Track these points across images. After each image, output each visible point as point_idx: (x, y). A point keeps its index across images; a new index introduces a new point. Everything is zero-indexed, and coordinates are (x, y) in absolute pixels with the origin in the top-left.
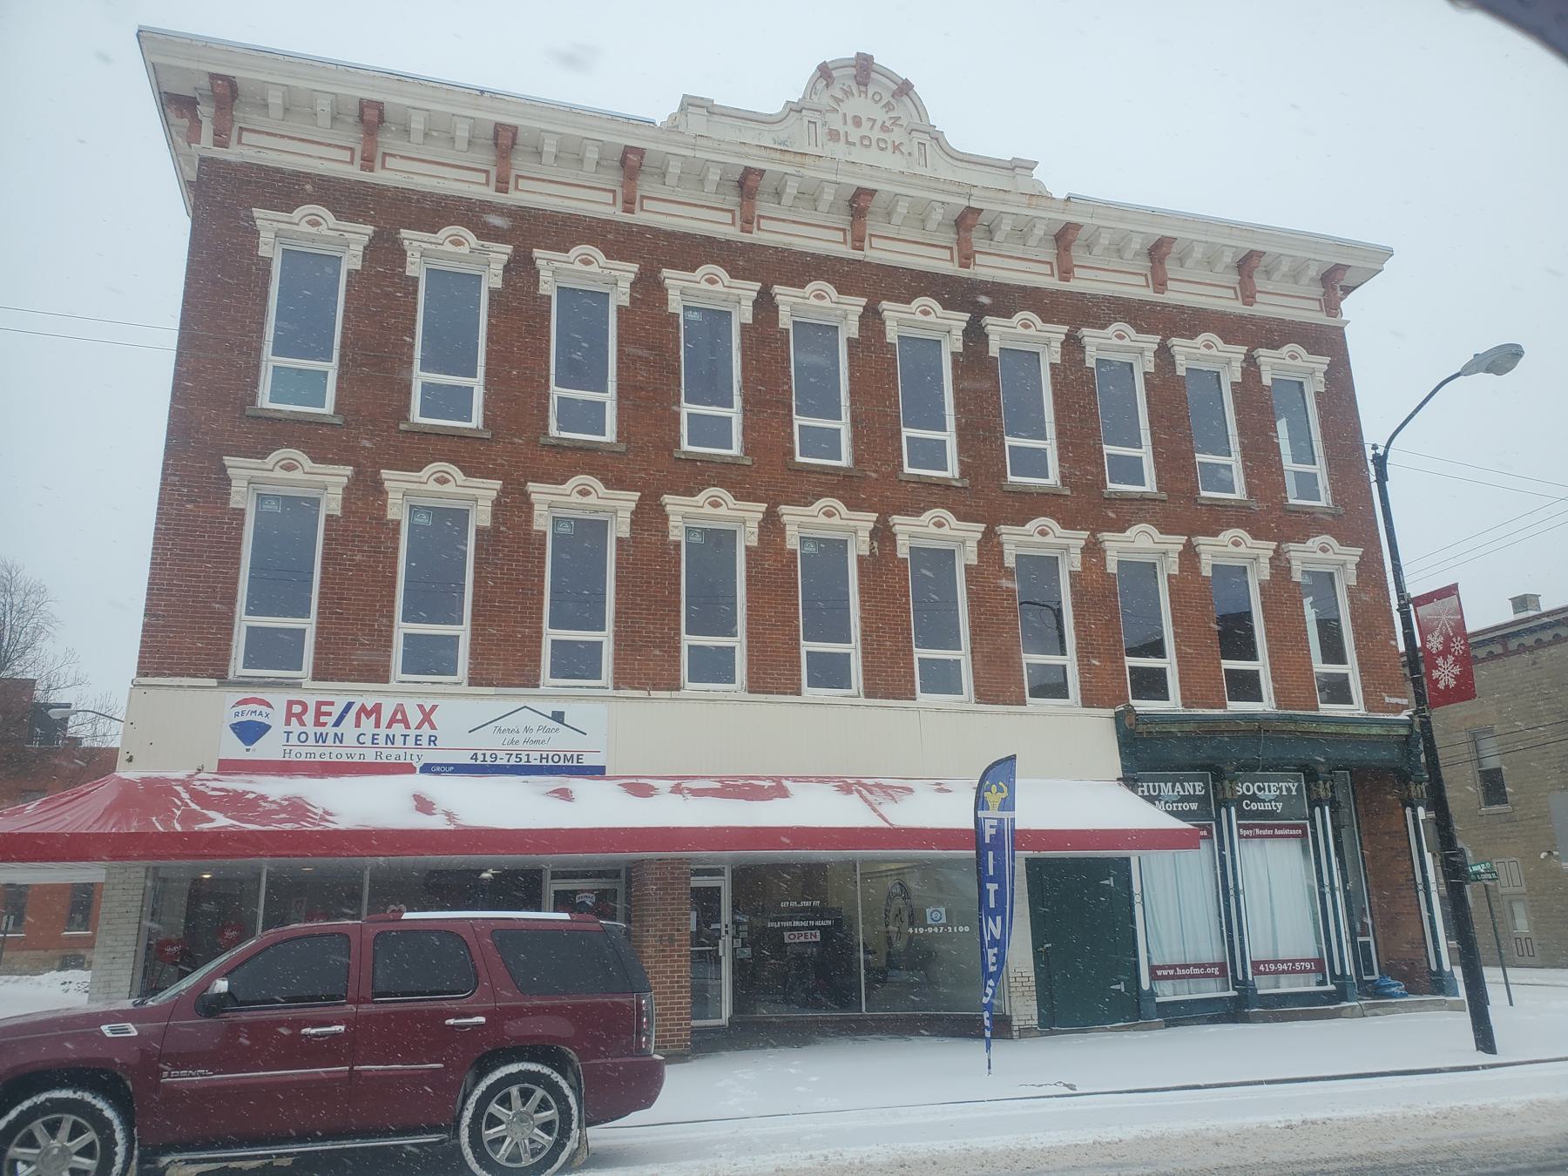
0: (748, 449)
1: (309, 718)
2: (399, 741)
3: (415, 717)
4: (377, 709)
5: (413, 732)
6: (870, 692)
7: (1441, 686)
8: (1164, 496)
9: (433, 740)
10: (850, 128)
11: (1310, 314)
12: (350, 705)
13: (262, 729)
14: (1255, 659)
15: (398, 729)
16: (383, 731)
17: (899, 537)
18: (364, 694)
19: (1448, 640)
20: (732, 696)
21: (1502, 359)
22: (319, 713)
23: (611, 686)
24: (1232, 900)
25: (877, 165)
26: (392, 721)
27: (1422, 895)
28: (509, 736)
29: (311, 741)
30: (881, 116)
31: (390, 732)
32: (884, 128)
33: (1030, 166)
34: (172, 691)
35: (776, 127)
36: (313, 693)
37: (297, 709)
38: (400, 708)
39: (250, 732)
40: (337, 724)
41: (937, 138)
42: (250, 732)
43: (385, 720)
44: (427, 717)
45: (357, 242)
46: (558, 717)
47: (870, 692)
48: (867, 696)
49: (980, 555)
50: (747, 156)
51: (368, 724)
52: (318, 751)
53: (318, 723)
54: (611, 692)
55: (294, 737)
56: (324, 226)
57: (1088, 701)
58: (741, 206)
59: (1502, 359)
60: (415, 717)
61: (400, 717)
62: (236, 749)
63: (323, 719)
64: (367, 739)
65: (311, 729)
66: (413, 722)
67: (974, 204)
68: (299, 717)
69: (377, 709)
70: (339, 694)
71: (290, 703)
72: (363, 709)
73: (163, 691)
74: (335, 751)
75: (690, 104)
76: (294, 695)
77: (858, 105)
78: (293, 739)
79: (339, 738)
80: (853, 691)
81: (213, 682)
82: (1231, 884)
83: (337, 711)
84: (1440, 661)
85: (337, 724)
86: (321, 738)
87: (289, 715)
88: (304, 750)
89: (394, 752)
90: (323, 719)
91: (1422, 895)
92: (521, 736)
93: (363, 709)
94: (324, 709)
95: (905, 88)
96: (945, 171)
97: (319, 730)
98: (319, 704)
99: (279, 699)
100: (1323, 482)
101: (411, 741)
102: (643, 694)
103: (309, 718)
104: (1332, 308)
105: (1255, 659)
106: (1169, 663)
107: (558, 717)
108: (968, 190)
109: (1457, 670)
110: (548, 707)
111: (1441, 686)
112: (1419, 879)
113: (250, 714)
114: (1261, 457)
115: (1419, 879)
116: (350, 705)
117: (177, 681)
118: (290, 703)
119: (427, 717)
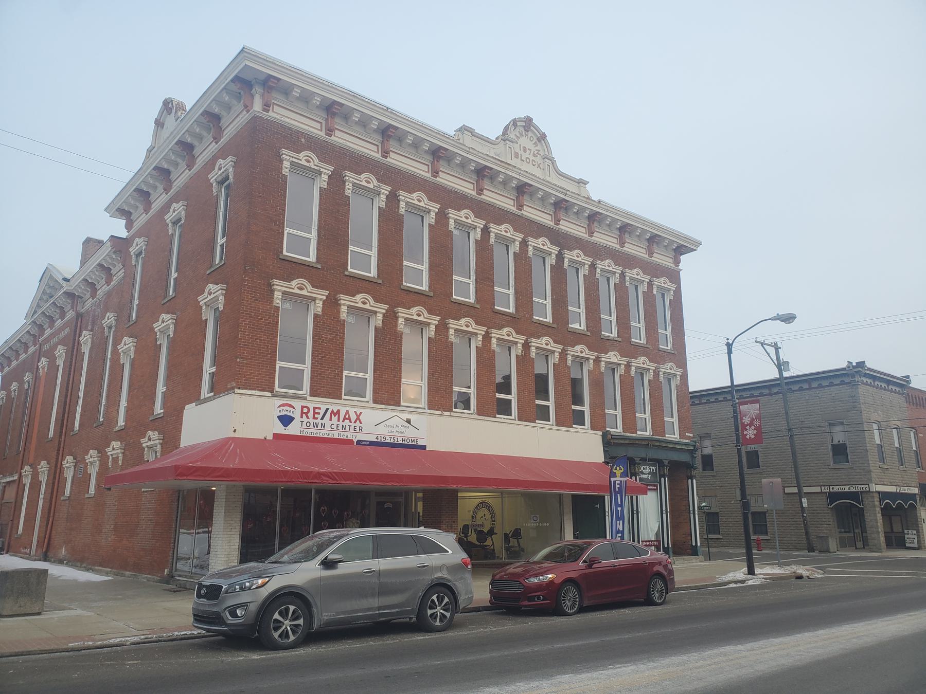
0: (478, 300)
1: (311, 415)
2: (347, 428)
3: (353, 417)
4: (338, 411)
5: (353, 425)
6: (558, 424)
7: (748, 437)
8: (620, 339)
9: (361, 429)
10: (522, 152)
11: (667, 262)
12: (327, 409)
13: (292, 419)
14: (510, 394)
15: (347, 421)
16: (341, 423)
17: (276, 293)
18: (332, 405)
19: (752, 420)
20: (367, 405)
21: (788, 319)
22: (315, 413)
23: (371, 402)
24: (635, 516)
25: (528, 169)
26: (345, 418)
27: (692, 515)
28: (391, 429)
29: (312, 426)
30: (533, 149)
31: (344, 424)
32: (534, 155)
33: (585, 183)
34: (252, 397)
35: (495, 147)
36: (313, 402)
37: (305, 410)
38: (347, 412)
39: (286, 420)
40: (322, 419)
41: (553, 161)
42: (286, 420)
43: (341, 419)
44: (358, 418)
45: (325, 174)
46: (409, 421)
47: (558, 424)
48: (519, 420)
49: (383, 322)
50: (487, 161)
51: (335, 419)
52: (315, 431)
53: (314, 418)
54: (371, 404)
55: (304, 424)
56: (312, 164)
57: (593, 428)
58: (326, 120)
59: (788, 319)
60: (353, 417)
61: (347, 418)
62: (280, 429)
63: (316, 416)
64: (334, 427)
65: (311, 420)
66: (353, 421)
67: (567, 198)
68: (306, 414)
69: (338, 411)
70: (323, 404)
71: (303, 407)
72: (332, 411)
73: (248, 397)
74: (322, 432)
75: (464, 129)
76: (304, 403)
77: (525, 141)
78: (304, 426)
79: (323, 426)
80: (550, 423)
81: (269, 394)
82: (635, 509)
83: (322, 412)
84: (748, 428)
85: (322, 419)
86: (316, 425)
87: (302, 413)
88: (309, 431)
89: (346, 434)
90: (316, 416)
91: (692, 515)
92: (395, 430)
93: (332, 411)
94: (317, 411)
95: (542, 137)
96: (554, 179)
97: (315, 421)
98: (315, 408)
99: (298, 404)
100: (670, 339)
101: (352, 428)
102: (439, 412)
103: (311, 415)
104: (677, 262)
105: (510, 394)
106: (513, 397)
107: (409, 421)
108: (565, 191)
109: (755, 432)
110: (406, 416)
111: (748, 437)
112: (691, 509)
113: (286, 411)
114: (485, 278)
115: (691, 509)
116: (327, 409)
117: (253, 392)
118: (303, 407)
119: (358, 418)
